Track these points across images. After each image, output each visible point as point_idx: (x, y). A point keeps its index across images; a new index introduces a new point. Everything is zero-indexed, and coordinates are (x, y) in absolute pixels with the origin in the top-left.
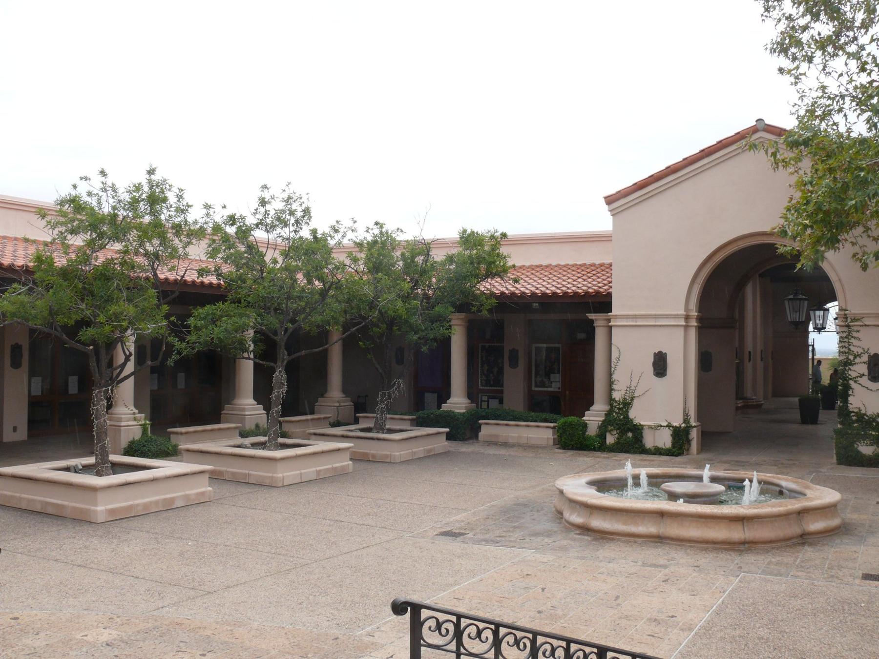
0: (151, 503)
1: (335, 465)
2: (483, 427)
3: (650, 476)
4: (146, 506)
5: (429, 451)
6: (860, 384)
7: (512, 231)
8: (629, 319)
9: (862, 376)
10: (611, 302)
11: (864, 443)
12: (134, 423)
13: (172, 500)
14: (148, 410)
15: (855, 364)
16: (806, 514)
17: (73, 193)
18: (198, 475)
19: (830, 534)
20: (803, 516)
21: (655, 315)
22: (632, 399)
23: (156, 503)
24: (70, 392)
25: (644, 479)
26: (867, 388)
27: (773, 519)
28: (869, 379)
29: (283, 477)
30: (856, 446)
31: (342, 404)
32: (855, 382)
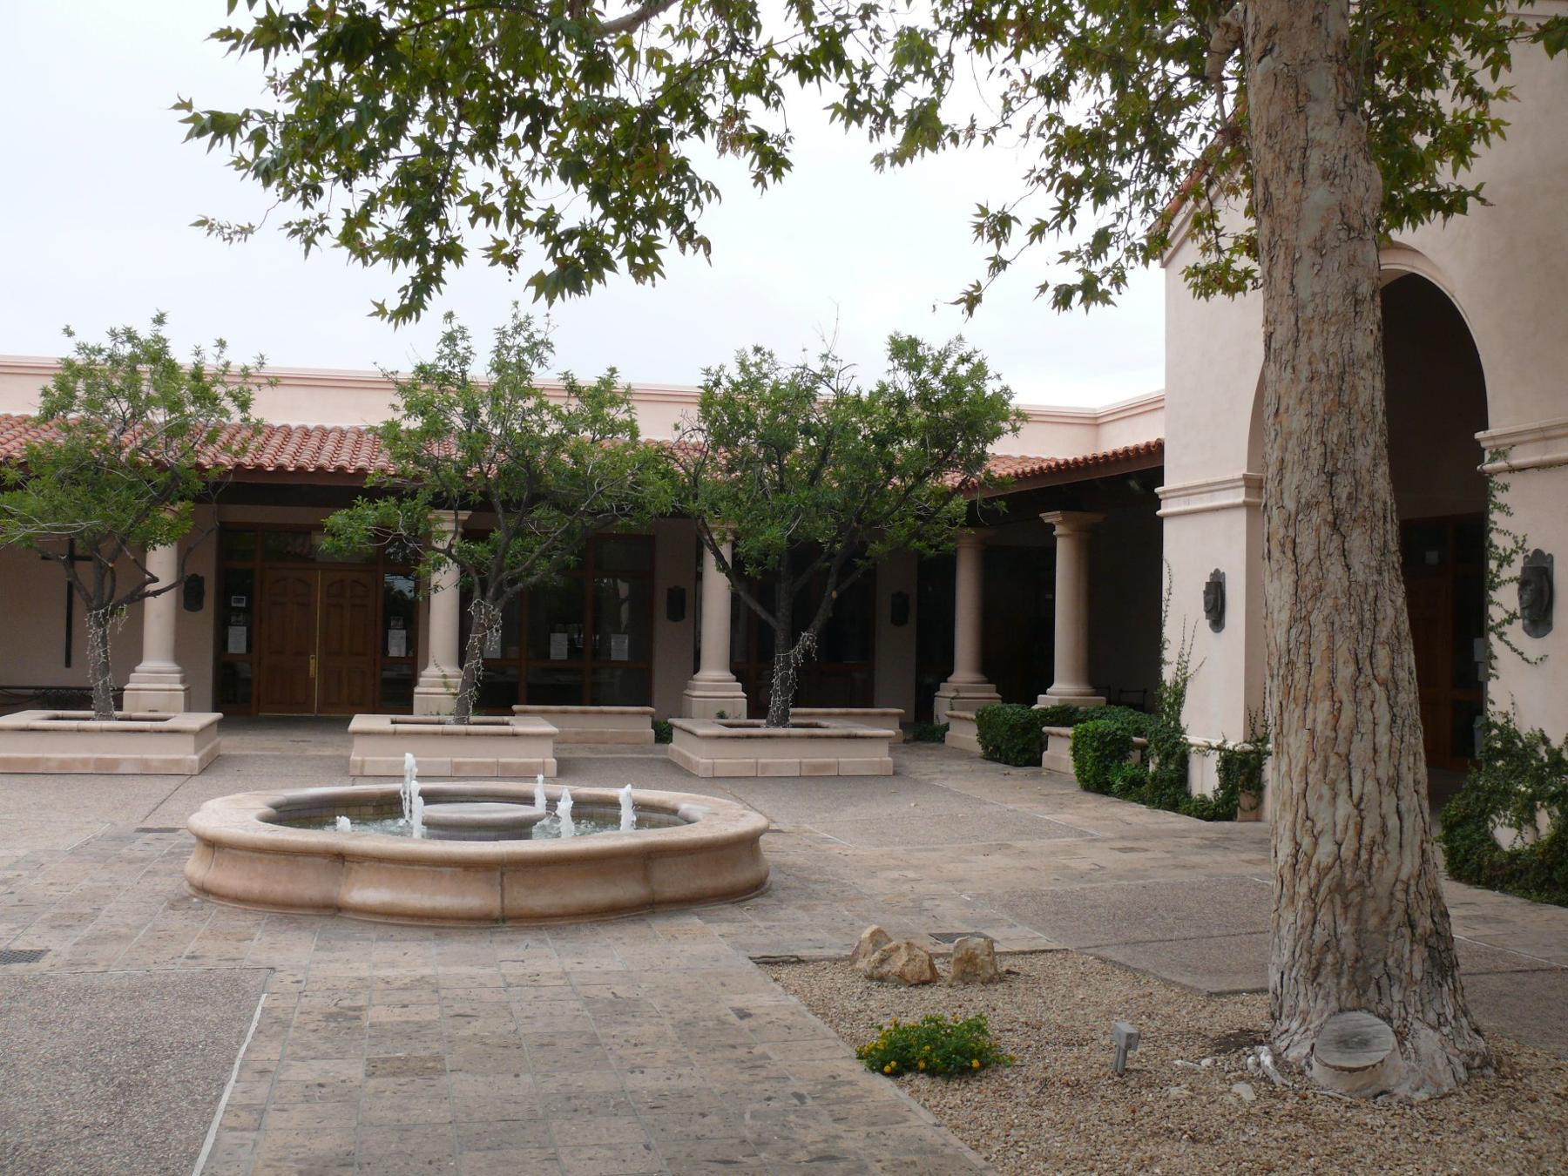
0: (74, 760)
1: (502, 760)
2: (1051, 741)
3: (640, 806)
4: (63, 763)
5: (816, 767)
6: (1508, 643)
7: (277, 363)
8: (1192, 498)
9: (1512, 617)
10: (1161, 469)
11: (1506, 816)
12: (443, 690)
13: (116, 762)
14: (913, 702)
15: (1500, 584)
16: (356, 866)
17: (991, 374)
18: (168, 735)
19: (390, 921)
20: (351, 869)
21: (1208, 485)
22: (1185, 680)
23: (85, 762)
24: (614, 657)
25: (565, 806)
26: (1521, 654)
27: (256, 855)
28: (1525, 629)
29: (363, 762)
30: (1491, 825)
31: (961, 695)
32: (1501, 636)
